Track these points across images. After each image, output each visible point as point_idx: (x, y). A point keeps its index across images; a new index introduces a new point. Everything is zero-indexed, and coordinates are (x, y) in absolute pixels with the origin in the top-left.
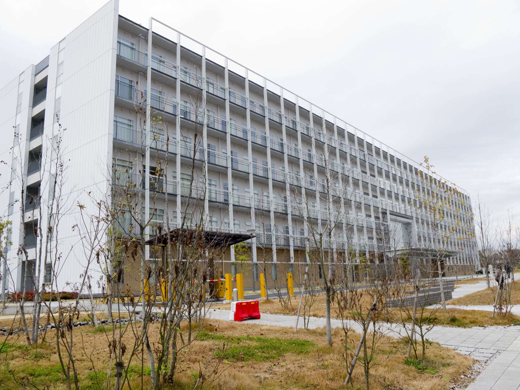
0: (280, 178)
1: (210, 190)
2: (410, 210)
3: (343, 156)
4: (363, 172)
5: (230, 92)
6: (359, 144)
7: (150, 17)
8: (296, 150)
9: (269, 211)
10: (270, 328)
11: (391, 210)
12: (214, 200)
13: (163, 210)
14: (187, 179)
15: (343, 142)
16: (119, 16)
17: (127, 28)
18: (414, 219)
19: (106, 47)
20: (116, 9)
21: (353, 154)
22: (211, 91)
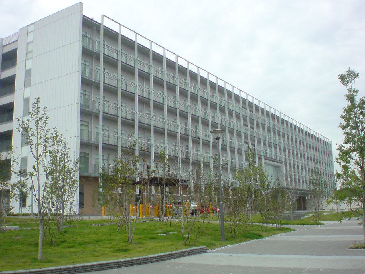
0: (160, 125)
1: (104, 134)
2: (281, 156)
3: (222, 110)
4: (244, 125)
5: (121, 52)
6: (243, 103)
7: (102, 14)
8: (175, 103)
9: (200, 161)
10: (288, 231)
11: (124, 115)
12: (205, 161)
13: (88, 154)
14: (85, 125)
15: (230, 102)
16: (83, 15)
17: (89, 25)
18: (284, 163)
19: (74, 38)
20: (81, 11)
21: (223, 105)
22: (106, 53)
